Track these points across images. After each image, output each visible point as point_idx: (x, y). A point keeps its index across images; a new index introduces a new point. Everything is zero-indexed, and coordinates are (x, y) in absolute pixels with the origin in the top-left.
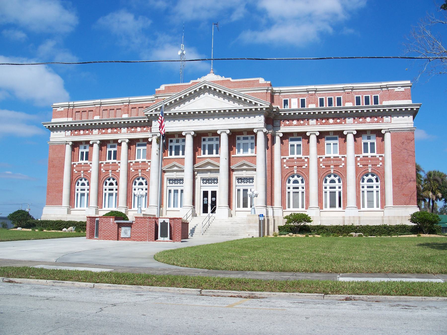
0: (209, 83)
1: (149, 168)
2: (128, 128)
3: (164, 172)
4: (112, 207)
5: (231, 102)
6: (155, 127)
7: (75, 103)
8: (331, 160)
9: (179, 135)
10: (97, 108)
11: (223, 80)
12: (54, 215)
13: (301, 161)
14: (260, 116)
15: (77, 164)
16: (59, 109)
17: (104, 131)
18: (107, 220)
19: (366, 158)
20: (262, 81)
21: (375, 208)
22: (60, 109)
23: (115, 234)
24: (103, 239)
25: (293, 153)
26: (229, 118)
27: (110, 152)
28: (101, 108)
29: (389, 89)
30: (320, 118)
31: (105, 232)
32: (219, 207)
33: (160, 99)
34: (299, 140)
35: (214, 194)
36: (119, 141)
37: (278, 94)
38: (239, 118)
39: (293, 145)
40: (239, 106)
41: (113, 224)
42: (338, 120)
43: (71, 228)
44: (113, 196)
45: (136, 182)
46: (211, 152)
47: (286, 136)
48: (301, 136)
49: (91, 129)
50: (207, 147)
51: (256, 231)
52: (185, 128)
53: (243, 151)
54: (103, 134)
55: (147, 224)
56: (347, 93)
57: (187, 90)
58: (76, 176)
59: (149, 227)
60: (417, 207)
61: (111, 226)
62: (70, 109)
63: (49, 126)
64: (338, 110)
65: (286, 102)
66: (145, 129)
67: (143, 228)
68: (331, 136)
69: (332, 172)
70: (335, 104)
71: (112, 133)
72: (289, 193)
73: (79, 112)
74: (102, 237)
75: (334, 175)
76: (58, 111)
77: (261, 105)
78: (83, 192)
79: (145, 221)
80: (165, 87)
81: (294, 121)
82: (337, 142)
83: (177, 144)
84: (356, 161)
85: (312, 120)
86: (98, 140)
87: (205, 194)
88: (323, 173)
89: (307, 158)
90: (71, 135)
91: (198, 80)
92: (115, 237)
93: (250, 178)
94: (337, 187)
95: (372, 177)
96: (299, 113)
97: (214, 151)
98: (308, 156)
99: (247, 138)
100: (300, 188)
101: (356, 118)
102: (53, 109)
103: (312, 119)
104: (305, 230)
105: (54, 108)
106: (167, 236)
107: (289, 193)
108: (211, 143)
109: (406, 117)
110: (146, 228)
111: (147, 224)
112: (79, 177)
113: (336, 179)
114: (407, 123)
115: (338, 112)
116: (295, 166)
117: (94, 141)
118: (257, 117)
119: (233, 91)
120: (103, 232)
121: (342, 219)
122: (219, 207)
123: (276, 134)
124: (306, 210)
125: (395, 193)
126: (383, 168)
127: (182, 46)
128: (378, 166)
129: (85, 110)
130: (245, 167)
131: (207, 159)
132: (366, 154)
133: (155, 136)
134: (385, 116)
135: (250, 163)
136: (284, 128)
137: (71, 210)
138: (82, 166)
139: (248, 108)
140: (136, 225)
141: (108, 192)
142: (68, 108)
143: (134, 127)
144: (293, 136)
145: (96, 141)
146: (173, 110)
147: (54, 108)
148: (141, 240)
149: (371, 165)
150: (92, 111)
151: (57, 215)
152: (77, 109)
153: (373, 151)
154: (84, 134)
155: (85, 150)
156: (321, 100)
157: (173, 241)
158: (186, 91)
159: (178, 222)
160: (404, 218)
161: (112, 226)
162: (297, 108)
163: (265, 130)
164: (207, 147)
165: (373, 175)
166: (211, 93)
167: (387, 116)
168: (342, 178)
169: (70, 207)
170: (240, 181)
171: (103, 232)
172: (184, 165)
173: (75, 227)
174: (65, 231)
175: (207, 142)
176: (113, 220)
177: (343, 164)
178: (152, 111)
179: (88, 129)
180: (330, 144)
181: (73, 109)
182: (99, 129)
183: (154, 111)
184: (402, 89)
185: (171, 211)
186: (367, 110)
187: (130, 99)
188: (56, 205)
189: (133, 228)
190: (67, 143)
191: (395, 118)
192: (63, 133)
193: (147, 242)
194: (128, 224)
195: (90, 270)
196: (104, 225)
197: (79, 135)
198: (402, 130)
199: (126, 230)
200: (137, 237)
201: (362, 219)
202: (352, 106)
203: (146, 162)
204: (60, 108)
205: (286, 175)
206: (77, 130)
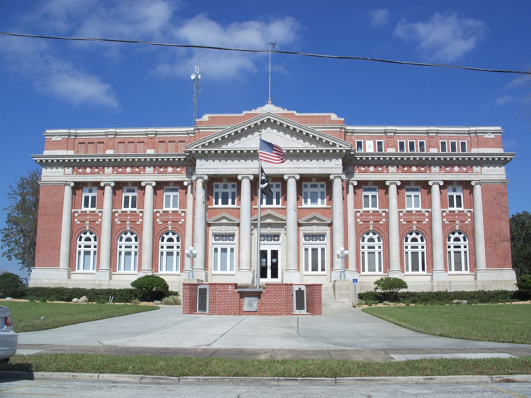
0: (274, 116)
2: (155, 168)
3: (208, 225)
5: (301, 141)
6: (199, 167)
7: (78, 131)
9: (228, 178)
10: (110, 139)
11: (285, 113)
12: (49, 280)
14: (337, 159)
15: (80, 212)
16: (54, 139)
17: (120, 170)
18: (223, 288)
19: (452, 213)
20: (334, 117)
21: (421, 271)
22: (57, 138)
23: (236, 306)
24: (217, 314)
25: (367, 205)
26: (298, 160)
27: (127, 198)
28: (116, 139)
29: (478, 135)
30: (401, 166)
31: (220, 305)
32: (286, 270)
33: (202, 132)
34: (374, 190)
35: (275, 254)
37: (351, 134)
38: (311, 161)
39: (368, 196)
40: (310, 146)
41: (232, 293)
42: (423, 168)
43: (84, 298)
44: (131, 255)
45: (122, 238)
46: (225, 202)
47: (362, 185)
48: (377, 185)
49: (101, 166)
50: (220, 195)
51: (348, 299)
52: (242, 170)
53: (311, 202)
54: (118, 173)
55: (283, 292)
56: (432, 137)
57: (245, 123)
58: (79, 229)
60: (512, 270)
61: (230, 297)
62: (71, 138)
63: (41, 161)
64: (424, 157)
65: (359, 144)
66: (178, 169)
67: (278, 299)
68: (413, 186)
69: (414, 228)
70: (417, 149)
71: (131, 173)
73: (84, 143)
74: (217, 311)
75: (172, 233)
76: (53, 141)
77: (340, 146)
79: (280, 289)
80: (209, 117)
81: (371, 167)
82: (418, 193)
83: (225, 190)
85: (392, 167)
86: (72, 182)
87: (263, 254)
88: (404, 230)
90: (73, 173)
91: (253, 111)
92: (237, 311)
93: (320, 235)
95: (459, 235)
96: (145, 159)
97: (230, 201)
99: (315, 186)
100: (377, 247)
101: (442, 167)
102: (46, 137)
103: (392, 165)
104: (395, 298)
105: (46, 136)
106: (303, 309)
107: (363, 253)
109: (497, 168)
110: (281, 299)
111: (283, 292)
112: (82, 229)
113: (419, 237)
114: (499, 175)
115: (424, 159)
116: (371, 221)
117: (107, 183)
118: (334, 160)
119: (305, 128)
120: (217, 305)
122: (286, 270)
123: (350, 182)
125: (487, 255)
127: (197, 68)
128: (466, 222)
129: (92, 141)
130: (315, 221)
131: (268, 210)
132: (126, 209)
133: (201, 178)
134: (475, 165)
135: (322, 216)
136: (359, 176)
137: (72, 274)
139: (324, 149)
140: (266, 294)
141: (83, 249)
142: (67, 137)
143: (164, 166)
144: (368, 185)
145: (109, 183)
146: (224, 146)
147: (46, 136)
148: (276, 314)
149: (458, 222)
150: (103, 143)
151: (53, 280)
152: (81, 139)
153: (459, 205)
154: (92, 173)
156: (402, 144)
157: (313, 314)
158: (244, 124)
159: (318, 289)
160: (500, 283)
161: (232, 297)
163: (344, 177)
164: (220, 195)
165: (460, 233)
166: (275, 129)
167: (477, 165)
168: (181, 238)
169: (70, 270)
171: (217, 305)
173: (113, 297)
174: (77, 302)
176: (232, 288)
178: (198, 147)
179: (98, 167)
180: (411, 196)
181: (75, 139)
182: (114, 167)
183: (200, 147)
184: (493, 136)
185: (218, 275)
186: (401, 158)
187: (78, 131)
188: (53, 266)
189: (262, 299)
190: (66, 184)
191: (486, 168)
192: (60, 170)
193: (284, 316)
194: (253, 294)
195: (444, 358)
196: (219, 295)
197: (124, 173)
198: (494, 182)
199: (250, 301)
200: (269, 310)
201: (452, 284)
202: (437, 152)
203: (179, 212)
204: (57, 136)
205: (360, 232)
206: (82, 167)
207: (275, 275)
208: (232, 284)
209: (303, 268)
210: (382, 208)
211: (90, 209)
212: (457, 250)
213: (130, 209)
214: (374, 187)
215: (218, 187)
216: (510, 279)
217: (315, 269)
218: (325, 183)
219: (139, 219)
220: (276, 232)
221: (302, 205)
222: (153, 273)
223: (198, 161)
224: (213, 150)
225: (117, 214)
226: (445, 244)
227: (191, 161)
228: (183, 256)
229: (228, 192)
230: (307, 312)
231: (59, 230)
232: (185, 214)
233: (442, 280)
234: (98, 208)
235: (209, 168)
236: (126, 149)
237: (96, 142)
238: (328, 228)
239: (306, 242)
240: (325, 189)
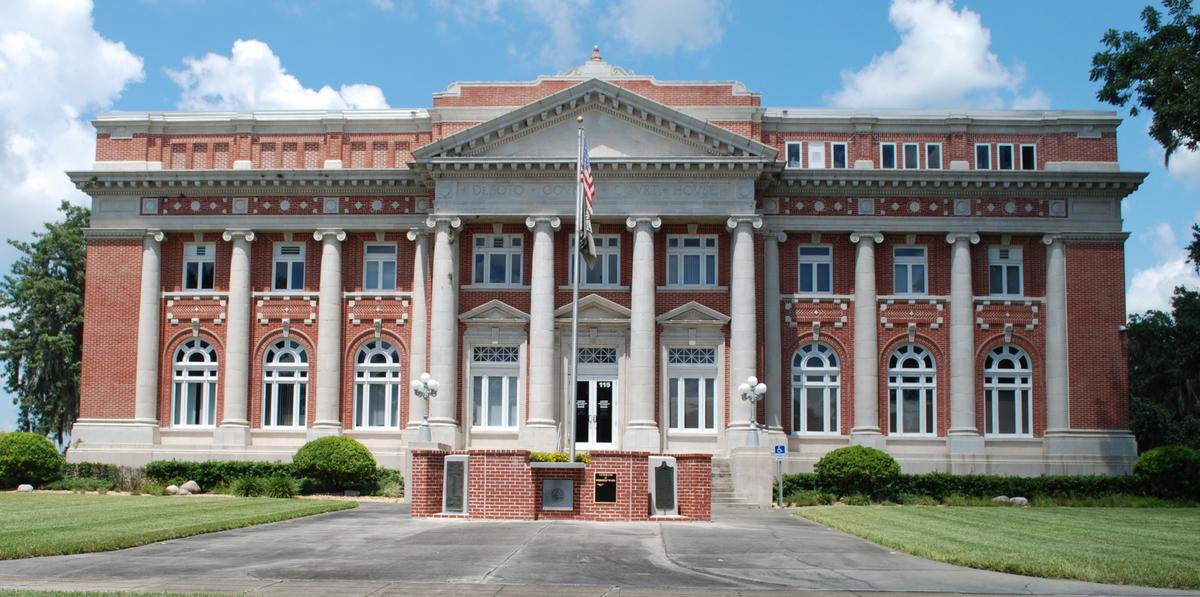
1: (313, 316)
4: (500, 424)
9: (504, 225)
13: (830, 309)
35: (605, 393)
36: (226, 237)
64: (843, 178)
65: (794, 153)
71: (292, 212)
72: (493, 383)
87: (582, 390)
89: (1039, 304)
98: (851, 297)
99: (695, 243)
116: (816, 320)
126: (1041, 331)
144: (810, 242)
155: (201, 257)
170: (677, 356)
172: (630, 308)
175: (681, 248)
188: (113, 416)
202: (872, 169)
204: (1091, 128)
207: (605, 435)
208: (519, 454)
209: (719, 419)
210: (1032, 295)
217: (692, 421)
218: (715, 237)
219: (309, 313)
221: (470, 283)
222: (340, 431)
225: (884, 307)
227: (424, 186)
228: (406, 394)
229: (505, 256)
230: (679, 513)
231: (134, 336)
234: (838, 290)
236: (392, 160)
239: (478, 363)
240: (522, 249)
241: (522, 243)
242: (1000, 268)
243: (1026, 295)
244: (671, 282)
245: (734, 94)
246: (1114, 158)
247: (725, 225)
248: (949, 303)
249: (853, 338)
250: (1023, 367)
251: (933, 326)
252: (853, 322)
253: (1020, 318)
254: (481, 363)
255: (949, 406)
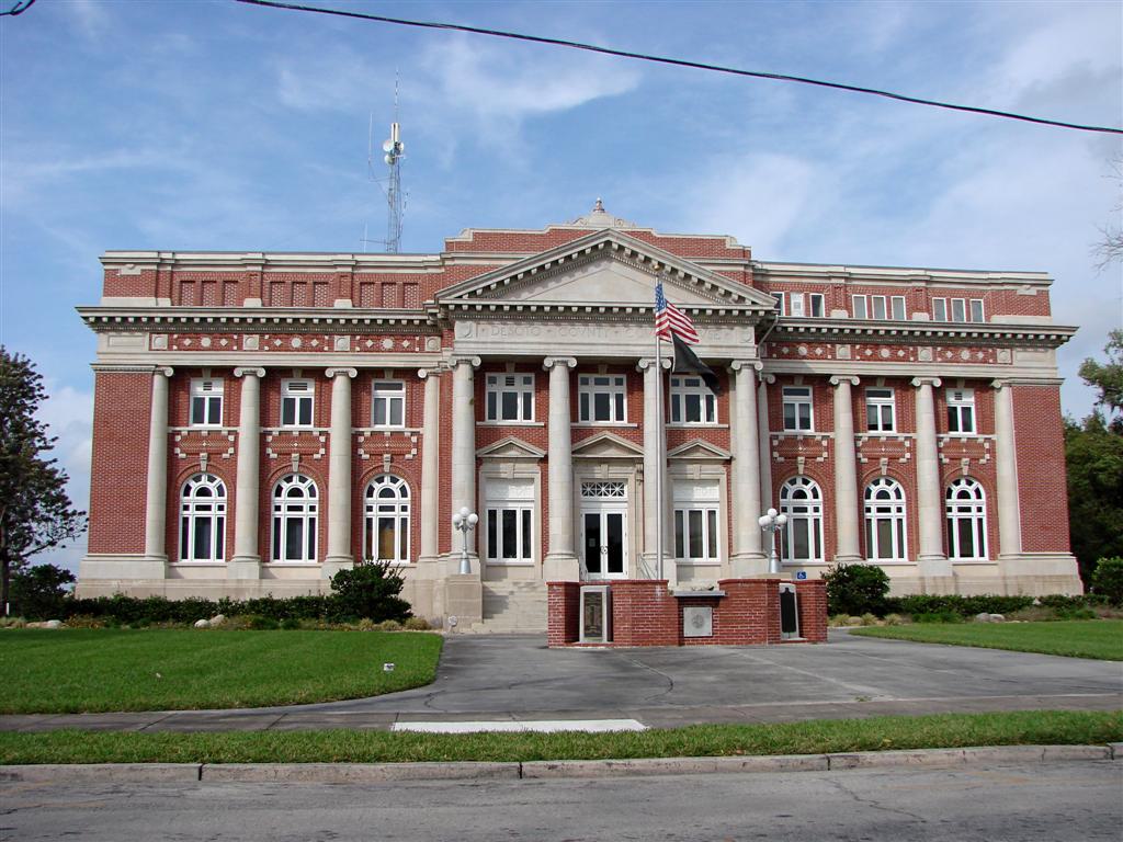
8: (880, 445)
52: (552, 347)
54: (865, 358)
59: (761, 610)
71: (303, 349)
77: (753, 303)
78: (295, 514)
83: (509, 389)
84: (772, 449)
94: (398, 508)
98: (831, 435)
99: (606, 382)
108: (602, 390)
121: (1000, 581)
124: (321, 564)
138: (880, 445)
139: (722, 307)
144: (793, 383)
151: (131, 580)
153: (967, 428)
154: (214, 348)
162: (803, 316)
170: (589, 489)
177: (908, 455)
178: (461, 297)
183: (465, 297)
188: (123, 551)
190: (158, 369)
207: (616, 565)
210: (983, 433)
211: (206, 426)
212: (884, 515)
213: (206, 426)
214: (396, 381)
215: (495, 383)
216: (1069, 573)
220: (619, 476)
221: (483, 420)
223: (458, 325)
224: (493, 303)
226: (860, 504)
230: (801, 636)
231: (143, 472)
232: (328, 439)
233: (942, 574)
234: (318, 424)
235: (483, 343)
237: (220, 281)
238: (722, 469)
241: (533, 382)
242: (955, 409)
243: (899, 432)
244: (582, 419)
245: (728, 247)
246: (1048, 314)
247: (542, 363)
248: (915, 440)
249: (834, 472)
250: (311, 496)
251: (224, 455)
252: (833, 458)
253: (810, 450)
254: (588, 497)
255: (918, 533)
